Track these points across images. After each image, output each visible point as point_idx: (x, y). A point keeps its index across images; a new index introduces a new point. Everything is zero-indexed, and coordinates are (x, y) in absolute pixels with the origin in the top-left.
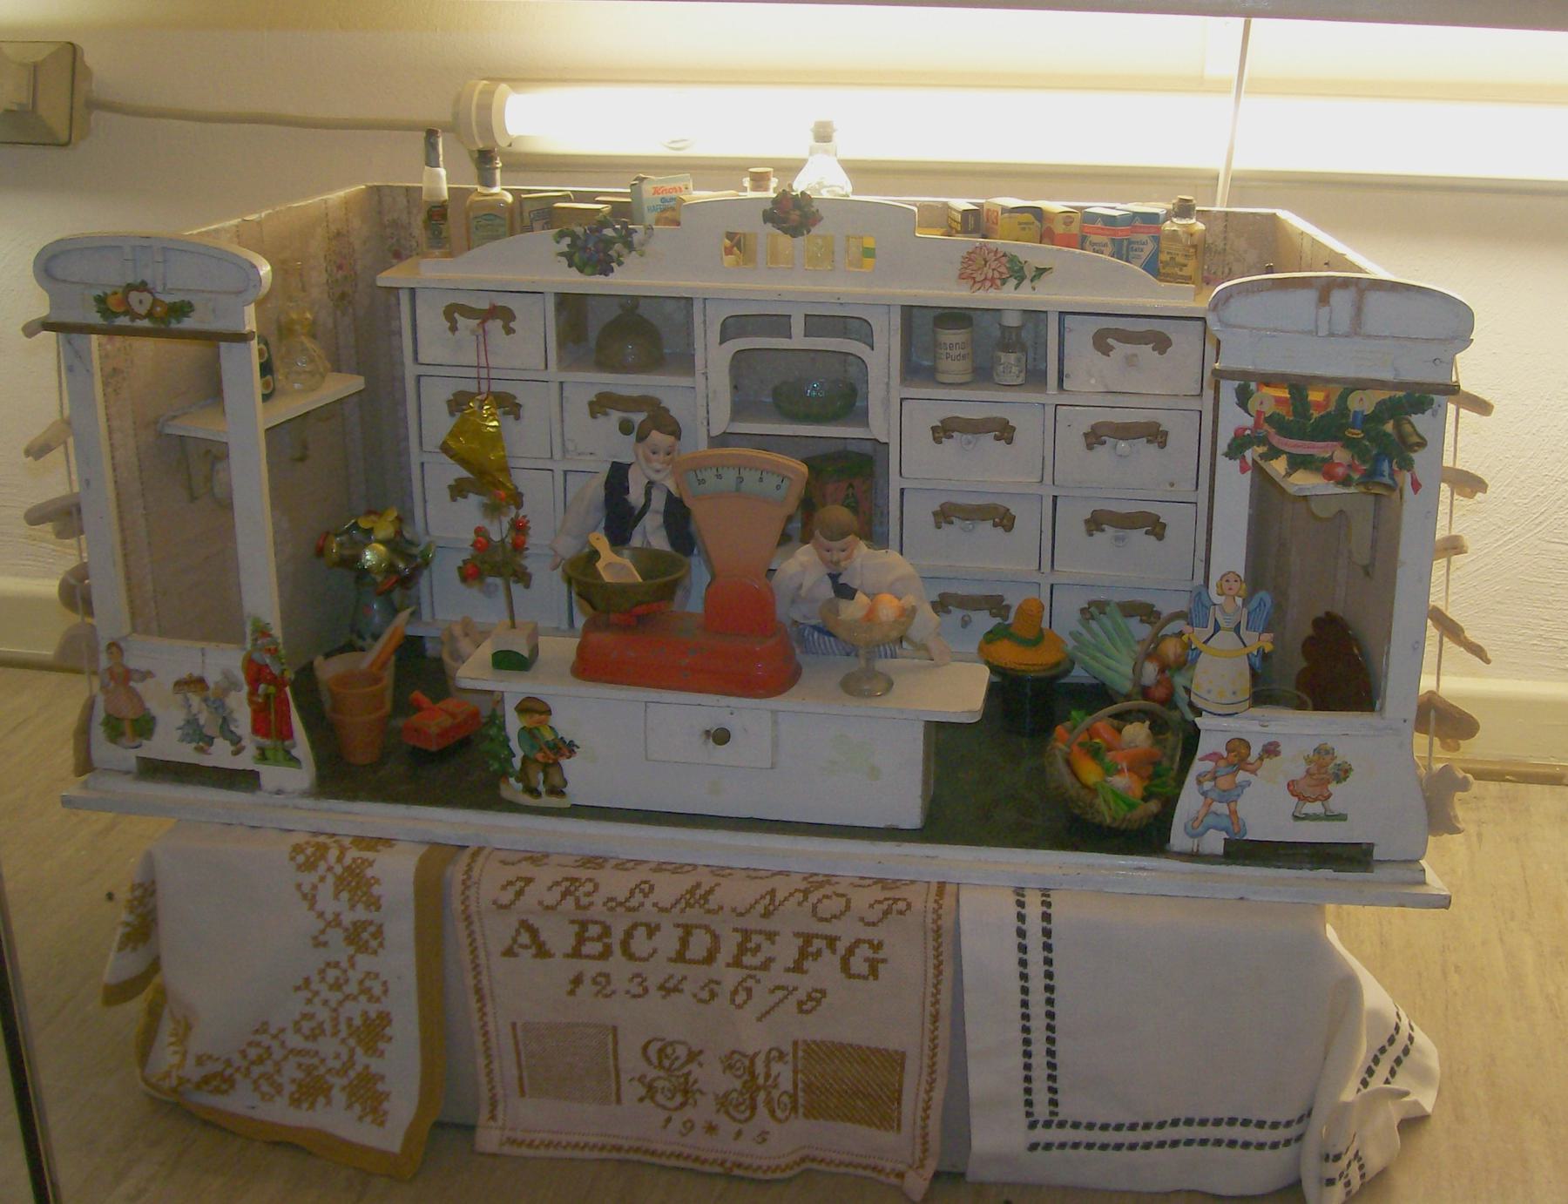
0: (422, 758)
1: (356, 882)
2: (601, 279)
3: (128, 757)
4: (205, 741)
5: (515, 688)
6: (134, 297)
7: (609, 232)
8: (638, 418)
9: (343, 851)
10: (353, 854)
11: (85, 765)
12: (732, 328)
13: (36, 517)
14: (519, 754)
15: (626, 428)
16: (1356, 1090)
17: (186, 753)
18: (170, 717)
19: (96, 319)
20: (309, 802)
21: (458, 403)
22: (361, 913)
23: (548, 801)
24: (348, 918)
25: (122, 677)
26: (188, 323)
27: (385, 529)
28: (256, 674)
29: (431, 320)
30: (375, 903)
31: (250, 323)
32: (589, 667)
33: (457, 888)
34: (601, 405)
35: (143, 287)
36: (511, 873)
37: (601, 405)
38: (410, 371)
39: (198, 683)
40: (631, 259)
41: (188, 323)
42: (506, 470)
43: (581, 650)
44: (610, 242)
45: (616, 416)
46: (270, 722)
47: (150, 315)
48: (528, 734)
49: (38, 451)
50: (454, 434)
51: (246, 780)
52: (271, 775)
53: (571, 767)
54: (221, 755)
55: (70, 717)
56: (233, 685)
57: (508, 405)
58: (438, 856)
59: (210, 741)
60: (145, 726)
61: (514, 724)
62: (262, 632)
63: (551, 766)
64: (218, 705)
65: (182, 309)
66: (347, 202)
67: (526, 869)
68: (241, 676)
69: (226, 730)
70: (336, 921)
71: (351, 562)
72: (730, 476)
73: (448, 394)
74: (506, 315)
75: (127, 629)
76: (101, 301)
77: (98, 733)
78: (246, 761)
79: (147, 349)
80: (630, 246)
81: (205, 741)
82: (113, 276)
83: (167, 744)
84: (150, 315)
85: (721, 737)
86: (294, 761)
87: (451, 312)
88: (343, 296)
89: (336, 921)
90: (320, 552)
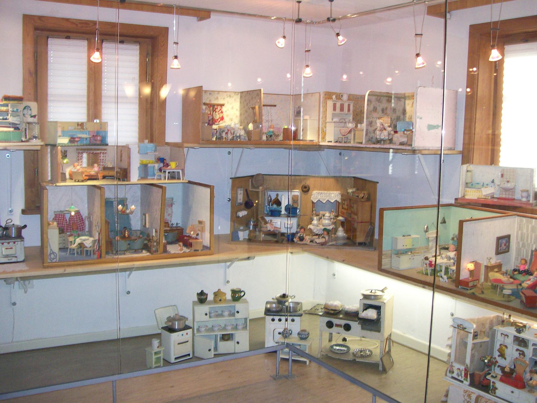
0: (483, 386)
1: (469, 396)
2: (519, 334)
3: (450, 375)
4: (459, 376)
5: (492, 380)
6: (461, 326)
7: (521, 329)
8: (521, 353)
9: (469, 392)
10: (470, 393)
11: (446, 375)
12: (534, 345)
13: (447, 345)
14: (491, 388)
15: (519, 354)
16: (449, 395)
17: (456, 377)
18: (456, 372)
19: (457, 327)
20: (468, 386)
21: (501, 345)
22: (469, 400)
23: (493, 394)
24: (468, 400)
25: (452, 366)
26: (466, 330)
27: (489, 358)
28: (465, 370)
29: (499, 334)
30: (471, 399)
31: (472, 331)
32: (501, 380)
33: (479, 400)
34: (517, 350)
35: (462, 325)
36: (486, 400)
37: (517, 350)
38: (496, 340)
39: (459, 369)
40: (523, 333)
41: (466, 330)
42: (504, 355)
43: (501, 378)
44: (521, 330)
45: (519, 352)
46: (466, 375)
47: (462, 328)
48: (493, 386)
49: (449, 338)
50: (499, 348)
51: (462, 382)
52: (465, 382)
53: (497, 391)
54: (460, 378)
55: (445, 369)
56: (463, 370)
57: (506, 347)
58: (478, 397)
59: (459, 376)
60: (453, 372)
61: (491, 384)
62: (467, 365)
63: (495, 390)
64: (461, 372)
65: (465, 328)
66: (493, 317)
67: (488, 401)
68: (464, 370)
69: (461, 375)
70: (466, 400)
71: (484, 361)
72: (520, 362)
73: (500, 344)
74: (508, 336)
75: (454, 361)
76: (458, 325)
77: (448, 372)
78: (462, 379)
79: (462, 332)
80: (523, 331)
81: (459, 376)
82: (460, 323)
83: (455, 375)
84: (462, 328)
85: (512, 392)
86: (467, 381)
87: (502, 334)
88: (491, 328)
89: (466, 400)
90: (481, 359)
